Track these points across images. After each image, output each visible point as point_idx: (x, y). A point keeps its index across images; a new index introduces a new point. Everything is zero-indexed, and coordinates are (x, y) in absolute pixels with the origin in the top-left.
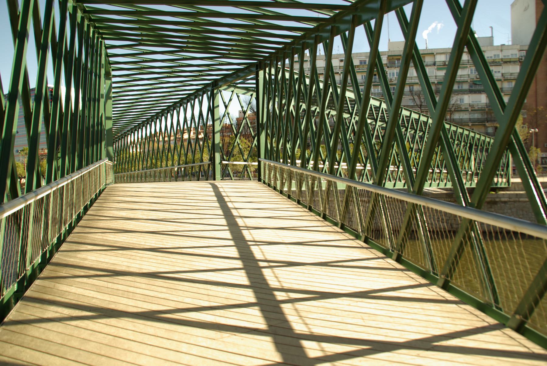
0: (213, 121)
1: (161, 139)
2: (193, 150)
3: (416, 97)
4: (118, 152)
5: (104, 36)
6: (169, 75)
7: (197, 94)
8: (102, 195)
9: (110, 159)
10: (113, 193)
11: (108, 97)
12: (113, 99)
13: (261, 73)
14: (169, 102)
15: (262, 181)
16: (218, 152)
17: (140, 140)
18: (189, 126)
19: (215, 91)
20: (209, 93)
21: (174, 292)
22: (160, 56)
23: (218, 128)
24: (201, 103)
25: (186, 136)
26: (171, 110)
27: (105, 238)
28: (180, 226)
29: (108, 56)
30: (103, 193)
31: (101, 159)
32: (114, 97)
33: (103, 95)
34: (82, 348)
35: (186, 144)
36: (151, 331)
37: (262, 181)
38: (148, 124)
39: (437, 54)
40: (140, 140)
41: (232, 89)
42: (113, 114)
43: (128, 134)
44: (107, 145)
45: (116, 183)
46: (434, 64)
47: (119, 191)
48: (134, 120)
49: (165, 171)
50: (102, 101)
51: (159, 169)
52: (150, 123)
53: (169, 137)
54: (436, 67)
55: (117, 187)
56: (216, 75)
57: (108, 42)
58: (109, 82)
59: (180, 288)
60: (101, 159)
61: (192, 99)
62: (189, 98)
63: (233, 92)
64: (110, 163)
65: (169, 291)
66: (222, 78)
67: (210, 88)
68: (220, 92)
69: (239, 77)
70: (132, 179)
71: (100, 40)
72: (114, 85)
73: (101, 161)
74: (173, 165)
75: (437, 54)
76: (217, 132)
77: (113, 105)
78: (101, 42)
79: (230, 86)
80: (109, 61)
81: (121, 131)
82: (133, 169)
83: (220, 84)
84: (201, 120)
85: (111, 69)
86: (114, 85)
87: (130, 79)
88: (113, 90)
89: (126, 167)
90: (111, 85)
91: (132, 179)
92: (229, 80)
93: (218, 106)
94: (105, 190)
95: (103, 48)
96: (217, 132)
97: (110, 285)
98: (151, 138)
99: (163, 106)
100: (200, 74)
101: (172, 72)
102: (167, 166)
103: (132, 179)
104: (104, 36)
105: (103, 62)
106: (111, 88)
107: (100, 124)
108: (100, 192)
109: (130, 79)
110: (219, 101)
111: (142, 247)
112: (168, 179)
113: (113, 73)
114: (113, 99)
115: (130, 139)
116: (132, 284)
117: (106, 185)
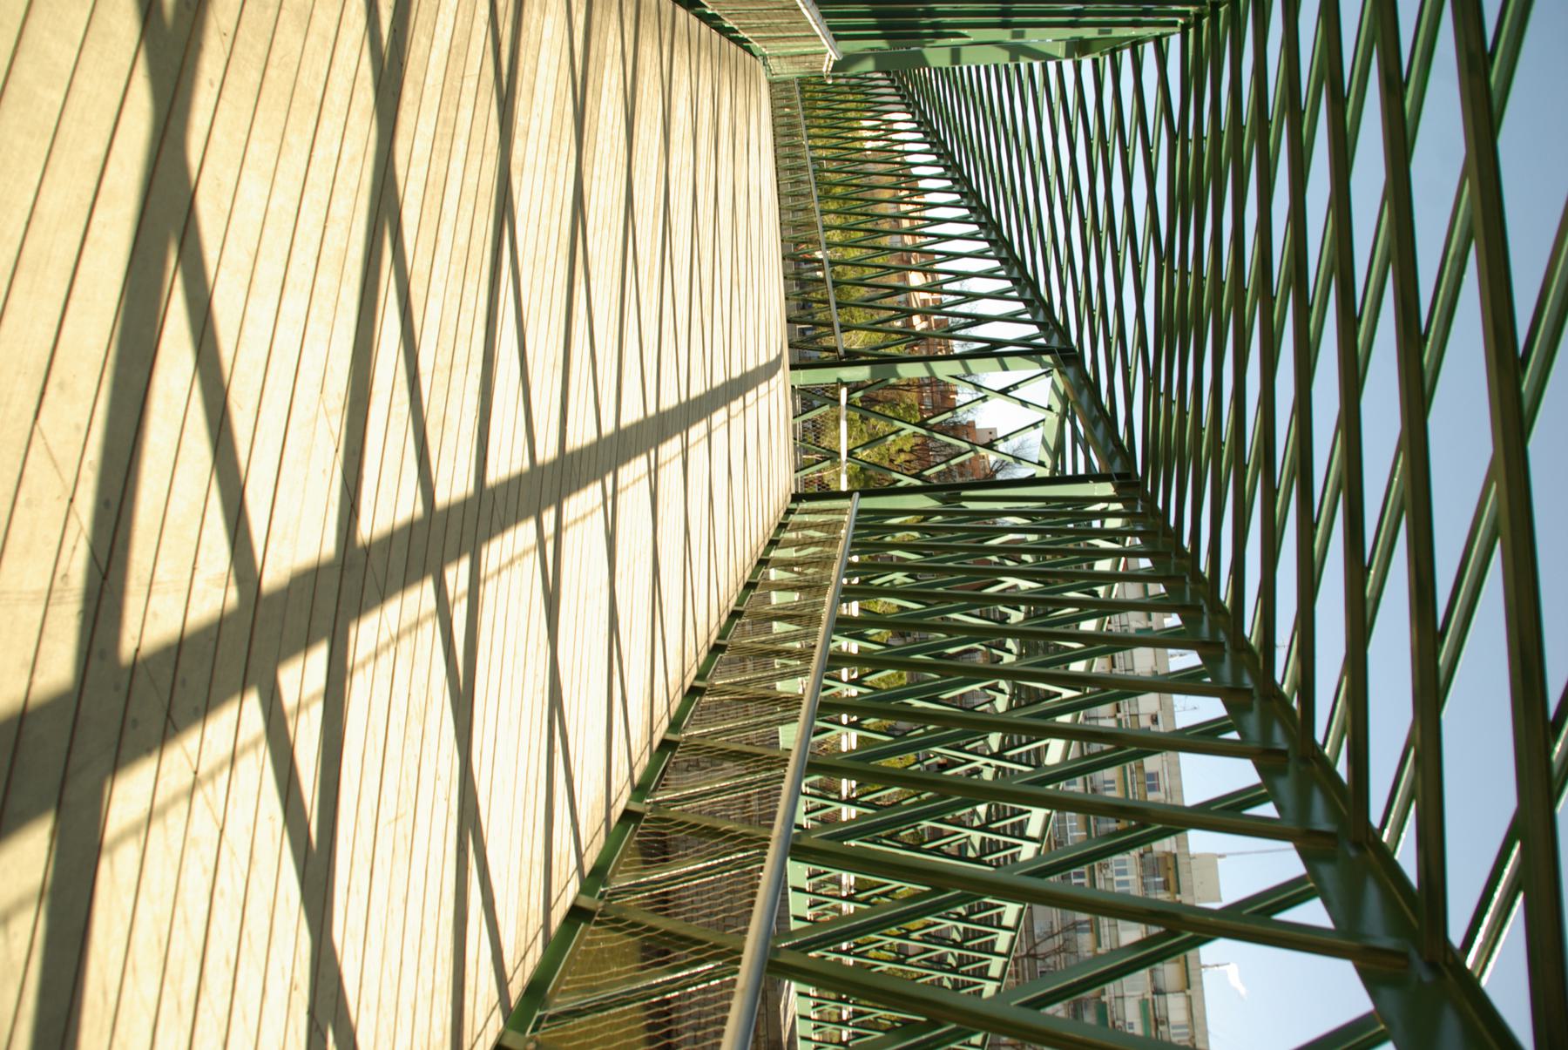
0: (962, 357)
1: (903, 208)
2: (878, 303)
3: (1058, 940)
4: (860, 86)
5: (1191, 31)
6: (1089, 222)
7: (1038, 306)
8: (733, 46)
9: (837, 66)
10: (741, 79)
11: (1016, 51)
12: (1011, 66)
13: (1107, 489)
14: (1010, 227)
15: (794, 506)
16: (873, 374)
17: (899, 148)
18: (946, 287)
19: (1047, 358)
20: (1042, 341)
21: (457, 268)
22: (1142, 194)
23: (943, 370)
24: (1011, 318)
25: (916, 279)
26: (989, 234)
27: (608, 61)
28: (650, 276)
29: (1135, 44)
30: (740, 51)
31: (837, 38)
32: (1018, 67)
33: (1021, 35)
34: (284, 14)
35: (894, 280)
36: (341, 208)
37: (794, 506)
38: (946, 167)
39: (1189, 998)
40: (899, 148)
41: (1057, 407)
42: (969, 69)
43: (913, 114)
44: (879, 57)
45: (772, 84)
46: (1158, 991)
47: (747, 96)
48: (955, 130)
49: (811, 225)
50: (1005, 35)
51: (816, 206)
52: (949, 174)
53: (911, 232)
54: (1149, 996)
55: (758, 90)
56: (1094, 357)
57: (1175, 43)
58: (1060, 51)
59: (471, 287)
60: (837, 38)
61: (1021, 293)
62: (1025, 284)
63: (1049, 408)
64: (827, 67)
65: (459, 255)
66: (1087, 377)
67: (1055, 342)
68: (1047, 373)
69: (1091, 424)
70: (784, 130)
71: (1181, 21)
72: (1052, 66)
73: (831, 40)
74: (830, 245)
75: (1189, 998)
76: (930, 369)
77: (996, 67)
78: (1174, 24)
79: (1064, 399)
80: (1121, 49)
81: (920, 92)
82: (813, 131)
83: (1071, 371)
84: (963, 320)
85: (1097, 55)
86: (1052, 66)
87: (1072, 113)
88: (1037, 65)
89: (820, 113)
90: (1052, 58)
91: (784, 132)
92: (1083, 398)
93: (1005, 368)
94: (748, 56)
95: (1157, 31)
96: (930, 369)
97: (470, 84)
98: (907, 180)
99: (999, 211)
100: (1097, 314)
101: (1097, 231)
102: (827, 228)
103: (784, 130)
104: (1191, 31)
105: (1118, 32)
106: (1044, 57)
107: (938, 32)
108: (740, 42)
109: (1072, 113)
110: (1021, 370)
111: (586, 169)
112: (790, 233)
113: (1087, 63)
114: (1011, 66)
115: (901, 119)
116: (476, 147)
117: (764, 57)
